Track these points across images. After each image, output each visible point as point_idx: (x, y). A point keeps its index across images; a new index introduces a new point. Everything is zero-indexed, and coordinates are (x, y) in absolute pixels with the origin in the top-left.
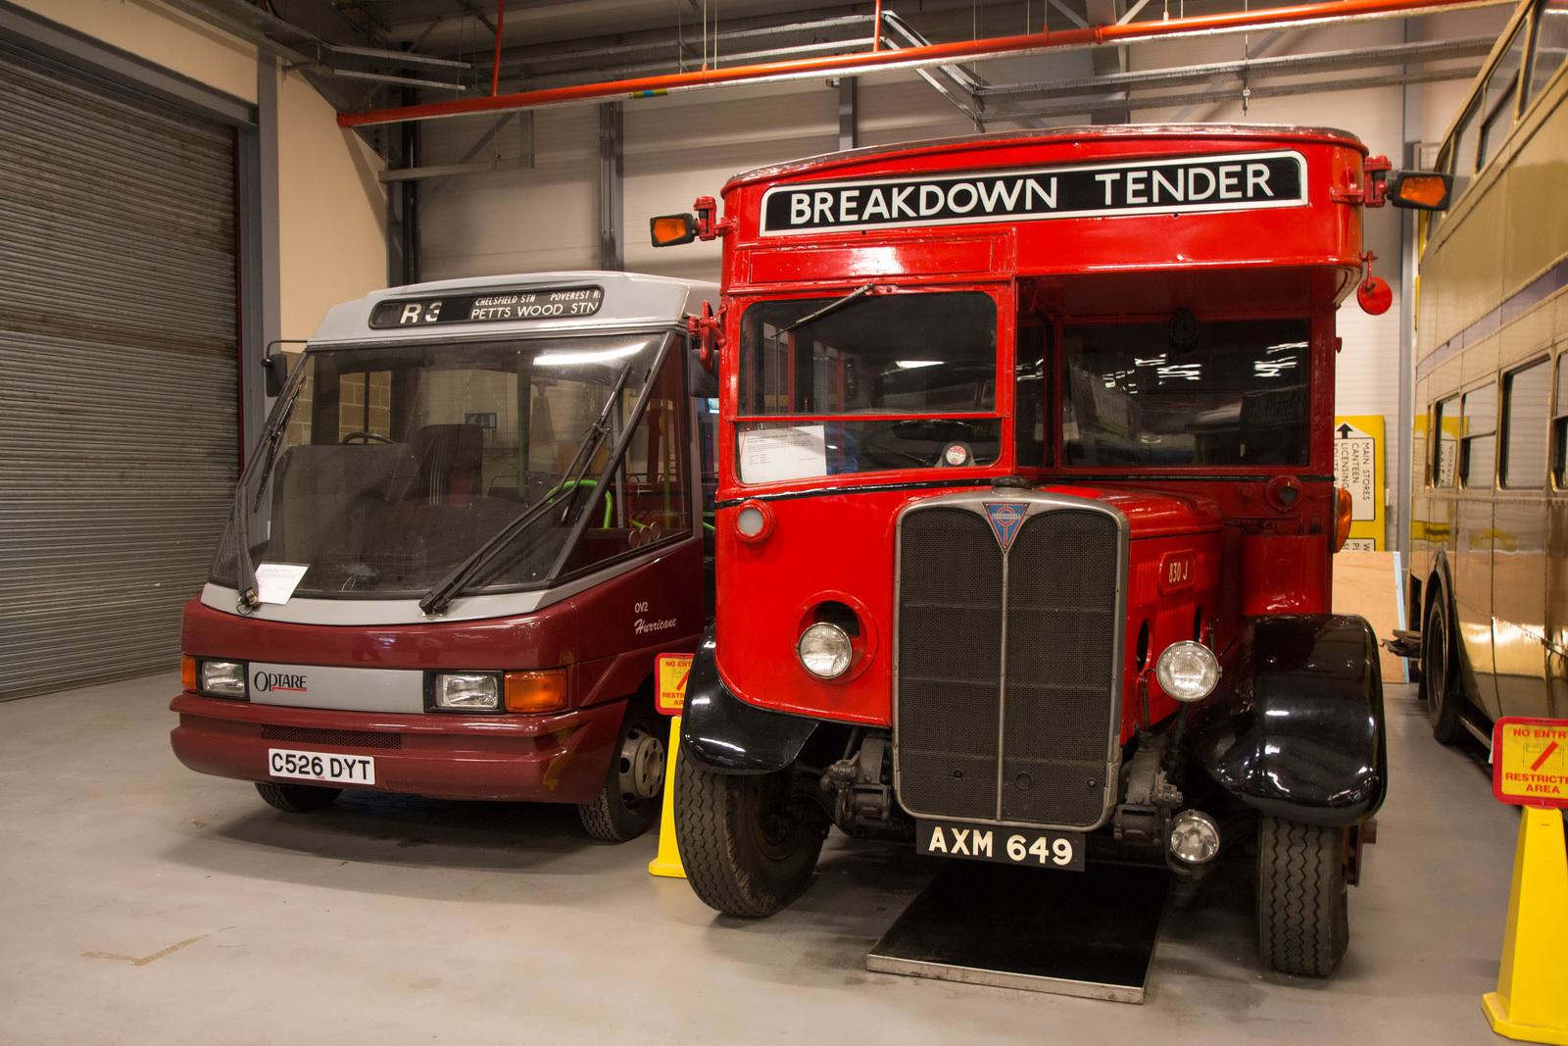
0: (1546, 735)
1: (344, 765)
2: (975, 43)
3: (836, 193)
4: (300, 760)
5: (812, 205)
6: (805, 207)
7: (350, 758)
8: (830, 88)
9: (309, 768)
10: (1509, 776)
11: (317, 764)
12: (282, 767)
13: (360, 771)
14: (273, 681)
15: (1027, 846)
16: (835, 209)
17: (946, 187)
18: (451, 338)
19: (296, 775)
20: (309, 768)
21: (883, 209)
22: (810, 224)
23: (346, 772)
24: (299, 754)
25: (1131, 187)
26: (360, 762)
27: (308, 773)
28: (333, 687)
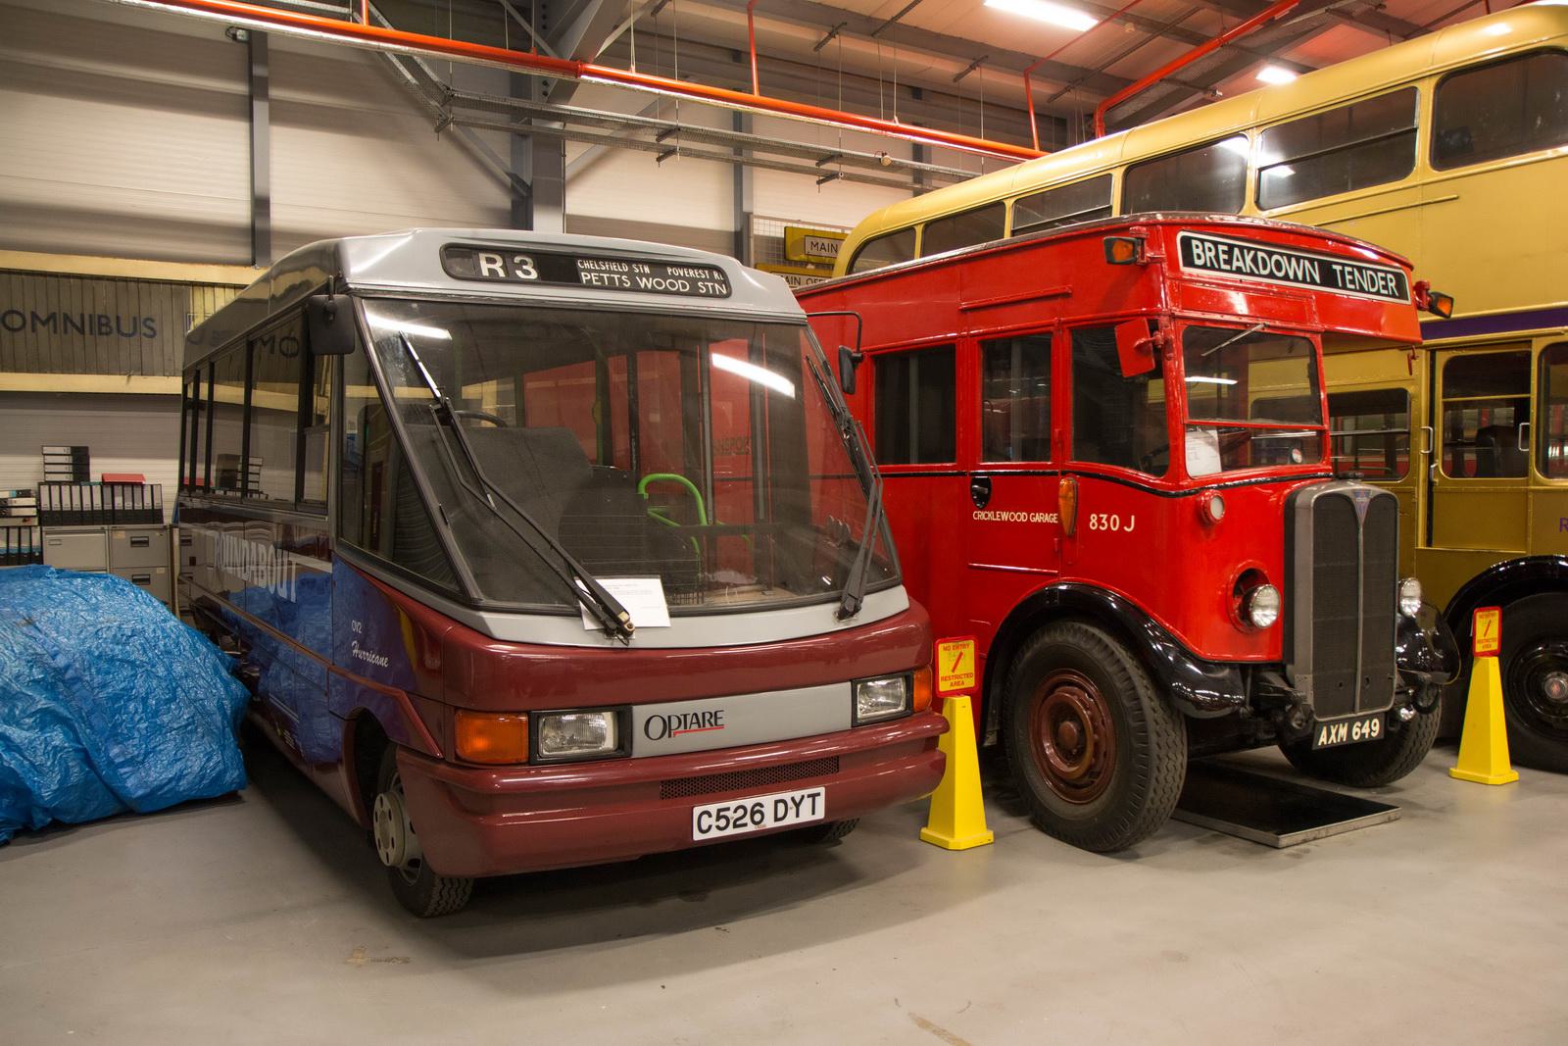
0: (957, 648)
1: (790, 804)
2: (450, 42)
3: (1231, 247)
4: (735, 811)
5: (1204, 251)
6: (1200, 251)
7: (797, 795)
8: (230, 41)
9: (747, 819)
10: (942, 678)
11: (758, 811)
12: (710, 827)
13: (808, 806)
14: (675, 723)
15: (1361, 728)
16: (1217, 256)
17: (1270, 254)
18: (590, 304)
19: (731, 831)
20: (747, 819)
21: (1240, 264)
22: (1204, 267)
23: (792, 812)
24: (733, 804)
25: (1348, 277)
26: (809, 796)
27: (745, 825)
28: (756, 718)
